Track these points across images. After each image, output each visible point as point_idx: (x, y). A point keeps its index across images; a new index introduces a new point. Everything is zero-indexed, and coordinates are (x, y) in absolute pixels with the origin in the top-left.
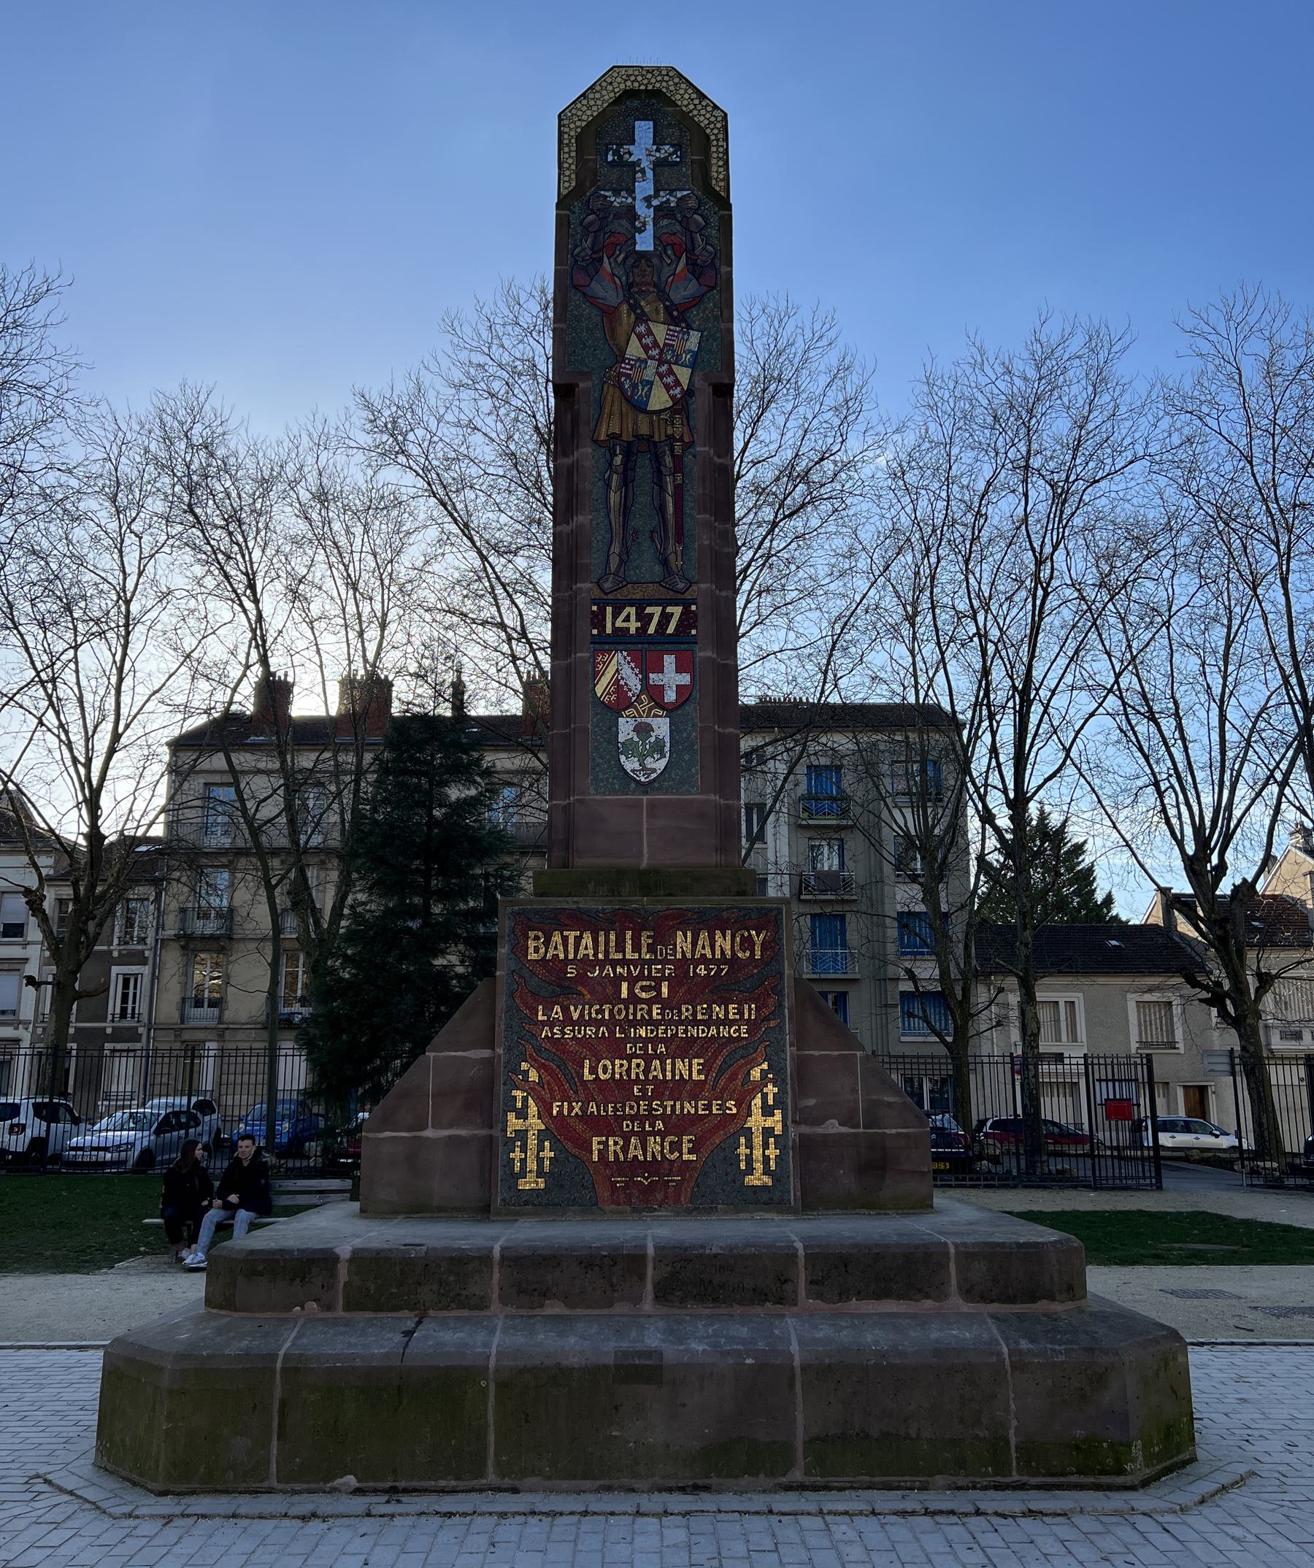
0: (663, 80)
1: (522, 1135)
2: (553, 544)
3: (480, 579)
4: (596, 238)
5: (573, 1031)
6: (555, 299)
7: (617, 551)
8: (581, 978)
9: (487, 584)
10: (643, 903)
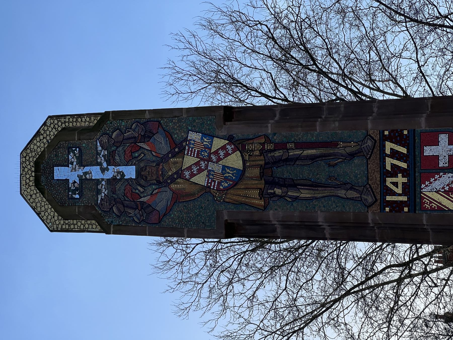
0: (29, 160)
2: (336, 240)
3: (363, 297)
4: (127, 207)
6: (165, 236)
7: (343, 192)
9: (367, 291)
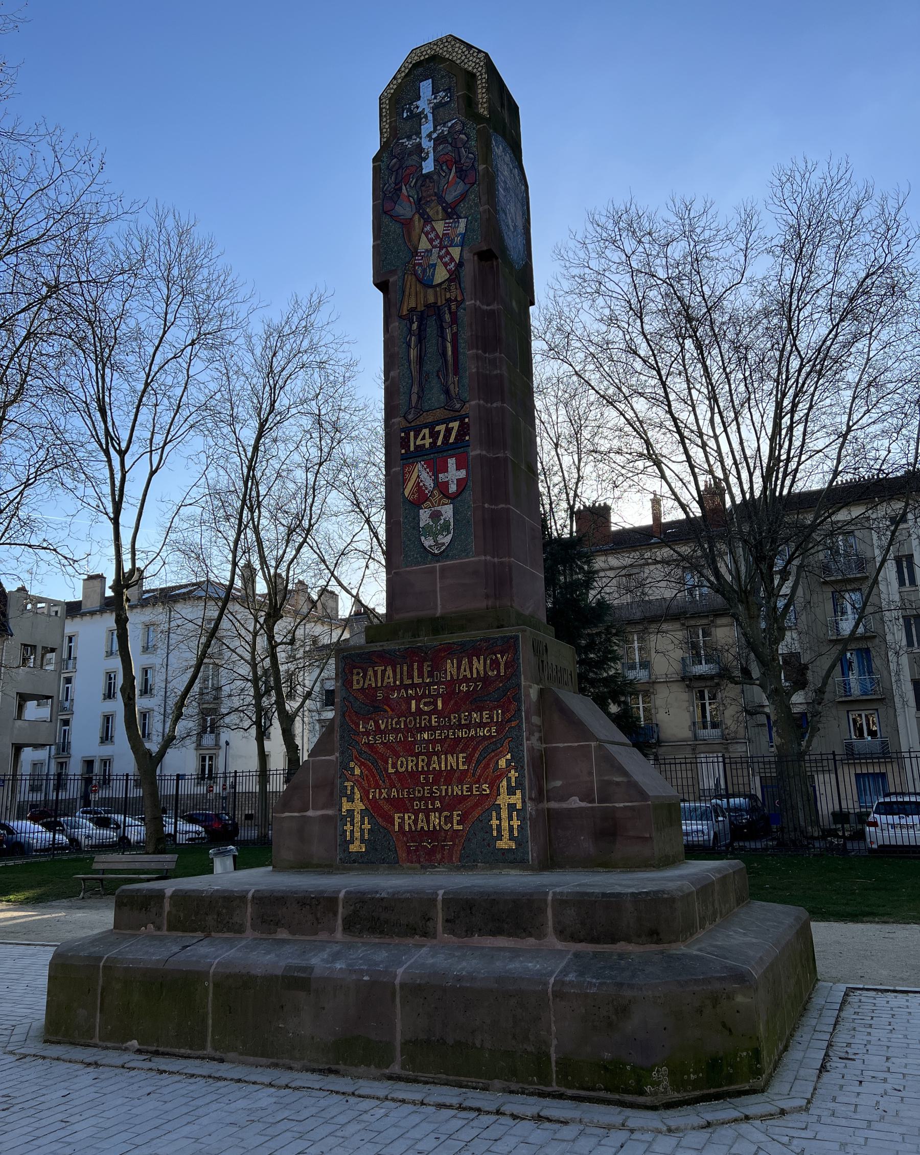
1: (351, 812)
5: (381, 738)
7: (416, 390)
8: (387, 700)
10: (425, 640)
